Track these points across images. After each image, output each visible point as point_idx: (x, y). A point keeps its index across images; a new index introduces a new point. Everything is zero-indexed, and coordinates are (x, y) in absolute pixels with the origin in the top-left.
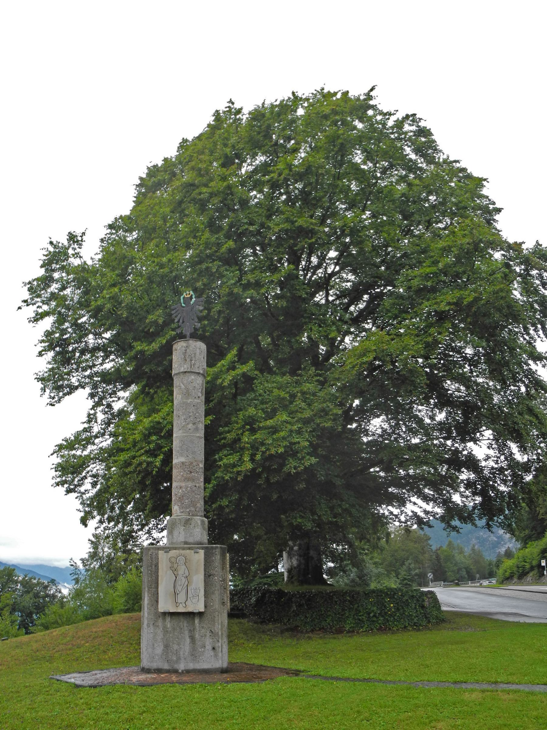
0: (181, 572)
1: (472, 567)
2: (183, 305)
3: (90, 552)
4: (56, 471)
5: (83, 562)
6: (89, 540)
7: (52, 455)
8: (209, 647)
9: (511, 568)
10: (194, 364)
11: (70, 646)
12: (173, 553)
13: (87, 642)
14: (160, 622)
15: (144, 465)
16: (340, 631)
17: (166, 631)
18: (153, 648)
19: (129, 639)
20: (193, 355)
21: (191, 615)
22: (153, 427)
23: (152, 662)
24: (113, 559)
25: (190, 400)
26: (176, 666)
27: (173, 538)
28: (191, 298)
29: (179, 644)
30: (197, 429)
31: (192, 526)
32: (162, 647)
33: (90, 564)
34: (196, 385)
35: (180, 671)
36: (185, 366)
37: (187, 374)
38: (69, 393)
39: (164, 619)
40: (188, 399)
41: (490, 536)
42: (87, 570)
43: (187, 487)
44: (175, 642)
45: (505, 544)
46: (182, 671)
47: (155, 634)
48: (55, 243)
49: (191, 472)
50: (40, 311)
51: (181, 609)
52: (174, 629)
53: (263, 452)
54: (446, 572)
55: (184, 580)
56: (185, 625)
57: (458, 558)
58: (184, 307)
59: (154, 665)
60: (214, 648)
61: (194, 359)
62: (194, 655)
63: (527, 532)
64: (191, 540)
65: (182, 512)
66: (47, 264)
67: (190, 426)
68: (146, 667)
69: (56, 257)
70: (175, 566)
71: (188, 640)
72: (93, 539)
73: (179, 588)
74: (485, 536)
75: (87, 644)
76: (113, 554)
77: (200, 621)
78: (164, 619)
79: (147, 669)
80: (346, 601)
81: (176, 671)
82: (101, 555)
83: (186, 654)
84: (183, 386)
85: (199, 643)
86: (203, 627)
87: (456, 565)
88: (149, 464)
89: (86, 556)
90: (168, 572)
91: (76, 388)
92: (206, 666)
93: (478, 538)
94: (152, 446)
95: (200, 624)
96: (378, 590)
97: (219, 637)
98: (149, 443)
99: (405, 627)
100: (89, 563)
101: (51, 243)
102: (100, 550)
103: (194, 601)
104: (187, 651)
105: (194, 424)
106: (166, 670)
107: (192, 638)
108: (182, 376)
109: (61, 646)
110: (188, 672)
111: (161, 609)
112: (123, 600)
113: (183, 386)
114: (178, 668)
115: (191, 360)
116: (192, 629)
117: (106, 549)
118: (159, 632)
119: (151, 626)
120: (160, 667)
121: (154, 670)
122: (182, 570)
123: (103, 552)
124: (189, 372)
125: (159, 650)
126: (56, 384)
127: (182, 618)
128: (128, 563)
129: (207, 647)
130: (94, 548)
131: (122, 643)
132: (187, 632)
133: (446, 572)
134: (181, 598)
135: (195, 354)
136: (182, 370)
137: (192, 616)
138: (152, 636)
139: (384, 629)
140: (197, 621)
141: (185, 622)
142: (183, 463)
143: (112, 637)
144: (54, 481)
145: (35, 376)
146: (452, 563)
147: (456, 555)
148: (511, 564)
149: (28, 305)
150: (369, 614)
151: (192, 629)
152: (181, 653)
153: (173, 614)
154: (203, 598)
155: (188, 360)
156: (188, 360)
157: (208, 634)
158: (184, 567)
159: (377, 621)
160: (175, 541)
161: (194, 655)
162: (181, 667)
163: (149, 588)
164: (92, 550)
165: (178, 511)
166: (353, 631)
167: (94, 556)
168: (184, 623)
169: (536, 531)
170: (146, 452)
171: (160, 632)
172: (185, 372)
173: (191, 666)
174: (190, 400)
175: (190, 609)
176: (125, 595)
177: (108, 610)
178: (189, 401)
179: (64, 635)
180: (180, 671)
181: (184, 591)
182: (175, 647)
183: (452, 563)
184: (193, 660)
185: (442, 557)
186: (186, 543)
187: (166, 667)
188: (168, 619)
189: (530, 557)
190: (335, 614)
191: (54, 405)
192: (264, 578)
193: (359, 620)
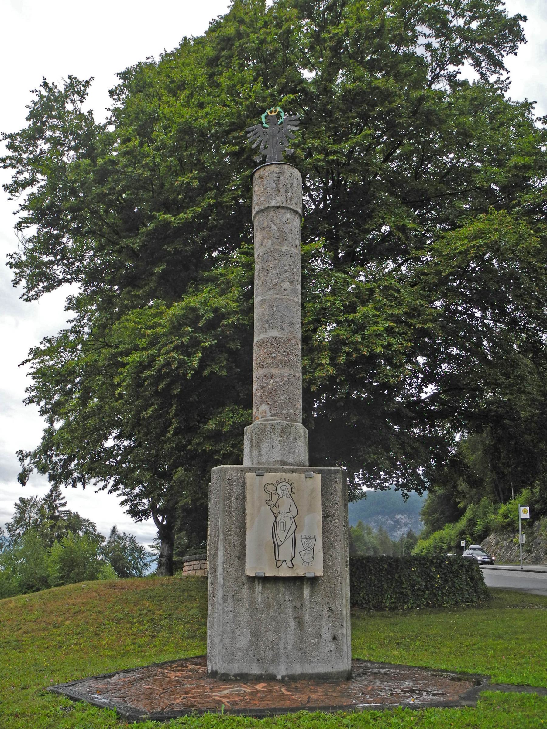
0: (284, 509)
1: (378, 547)
2: (265, 125)
3: (16, 517)
4: (34, 378)
5: (8, 528)
6: (16, 505)
7: (23, 364)
8: (327, 636)
9: (427, 548)
10: (291, 198)
11: (43, 625)
12: (269, 477)
13: (67, 619)
14: (245, 591)
15: (175, 365)
16: (379, 608)
17: (254, 609)
18: (234, 638)
19: (127, 615)
20: (289, 186)
21: (298, 581)
22: (185, 316)
23: (231, 662)
24: (39, 525)
25: (285, 248)
26: (272, 670)
27: (260, 455)
28: (278, 116)
29: (276, 631)
30: (294, 291)
31: (291, 437)
32: (248, 637)
33: (16, 530)
34: (293, 229)
35: (279, 677)
36: (278, 199)
37: (280, 210)
38: (48, 289)
39: (252, 588)
40: (281, 244)
41: (387, 520)
42: (12, 536)
43: (282, 377)
44: (270, 627)
45: (401, 528)
46: (283, 677)
47: (236, 614)
48: (50, 85)
49: (288, 354)
50: (21, 178)
51: (284, 572)
52: (269, 605)
53: (348, 354)
54: (357, 551)
55: (289, 522)
56: (287, 598)
57: (367, 538)
58: (266, 128)
59: (235, 668)
60: (335, 638)
61: (290, 190)
62: (303, 651)
63: (436, 516)
64: (290, 459)
65: (275, 415)
66: (33, 115)
67: (286, 285)
68: (221, 671)
69: (50, 106)
70: (275, 498)
71: (292, 624)
72: (21, 505)
73: (280, 536)
74: (383, 520)
75: (68, 622)
76: (39, 520)
77: (312, 592)
78: (252, 588)
79: (224, 674)
80: (382, 570)
81: (271, 678)
82: (27, 520)
83: (290, 647)
84: (274, 228)
85: (310, 630)
86: (316, 603)
87: (365, 543)
88: (182, 364)
89: (12, 521)
90: (263, 508)
91: (60, 282)
92: (322, 669)
93: (377, 521)
94: (186, 340)
95: (311, 597)
96: (420, 557)
97: (343, 619)
98: (181, 336)
99: (457, 603)
100: (14, 528)
101: (46, 84)
102: (26, 516)
103: (306, 558)
104: (291, 643)
105: (291, 283)
106: (255, 675)
107: (299, 620)
108: (272, 213)
109: (29, 624)
110: (293, 678)
111: (250, 572)
112: (58, 566)
113: (274, 228)
114: (275, 672)
115: (287, 192)
116: (299, 605)
117: (32, 515)
118: (243, 610)
119: (230, 600)
120: (245, 671)
121: (235, 676)
122: (285, 505)
123: (30, 517)
124: (283, 208)
125: (243, 641)
126: (34, 274)
127: (281, 587)
128: (54, 530)
129: (324, 636)
130: (20, 513)
131: (118, 621)
132: (290, 611)
133: (357, 551)
134: (285, 552)
135: (292, 184)
136: (273, 203)
137: (298, 583)
138: (230, 616)
139: (435, 605)
140: (306, 591)
141: (287, 593)
142: (275, 339)
143: (100, 612)
144: (27, 395)
145: (8, 260)
146: (361, 543)
147: (365, 535)
148: (427, 545)
149: (5, 167)
150: (413, 586)
151: (299, 605)
152: (281, 646)
153: (265, 580)
154: (321, 554)
155: (283, 191)
156: (283, 191)
157: (326, 613)
158: (290, 500)
159: (423, 596)
160: (264, 460)
161: (303, 651)
162: (281, 671)
163: (227, 535)
164: (18, 515)
165: (268, 413)
166: (396, 608)
167: (19, 521)
168: (285, 595)
169: (444, 514)
170: (176, 348)
171: (244, 610)
172: (278, 207)
173: (298, 669)
174: (285, 248)
175: (300, 572)
176: (60, 562)
177: (43, 577)
178: (284, 249)
179: (27, 608)
180: (279, 677)
181: (290, 541)
182: (271, 636)
183: (361, 543)
184: (301, 658)
185: (353, 536)
186: (283, 463)
187: (255, 670)
188: (259, 588)
189: (447, 538)
190: (370, 586)
191: (30, 301)
192: (199, 548)
193: (402, 593)
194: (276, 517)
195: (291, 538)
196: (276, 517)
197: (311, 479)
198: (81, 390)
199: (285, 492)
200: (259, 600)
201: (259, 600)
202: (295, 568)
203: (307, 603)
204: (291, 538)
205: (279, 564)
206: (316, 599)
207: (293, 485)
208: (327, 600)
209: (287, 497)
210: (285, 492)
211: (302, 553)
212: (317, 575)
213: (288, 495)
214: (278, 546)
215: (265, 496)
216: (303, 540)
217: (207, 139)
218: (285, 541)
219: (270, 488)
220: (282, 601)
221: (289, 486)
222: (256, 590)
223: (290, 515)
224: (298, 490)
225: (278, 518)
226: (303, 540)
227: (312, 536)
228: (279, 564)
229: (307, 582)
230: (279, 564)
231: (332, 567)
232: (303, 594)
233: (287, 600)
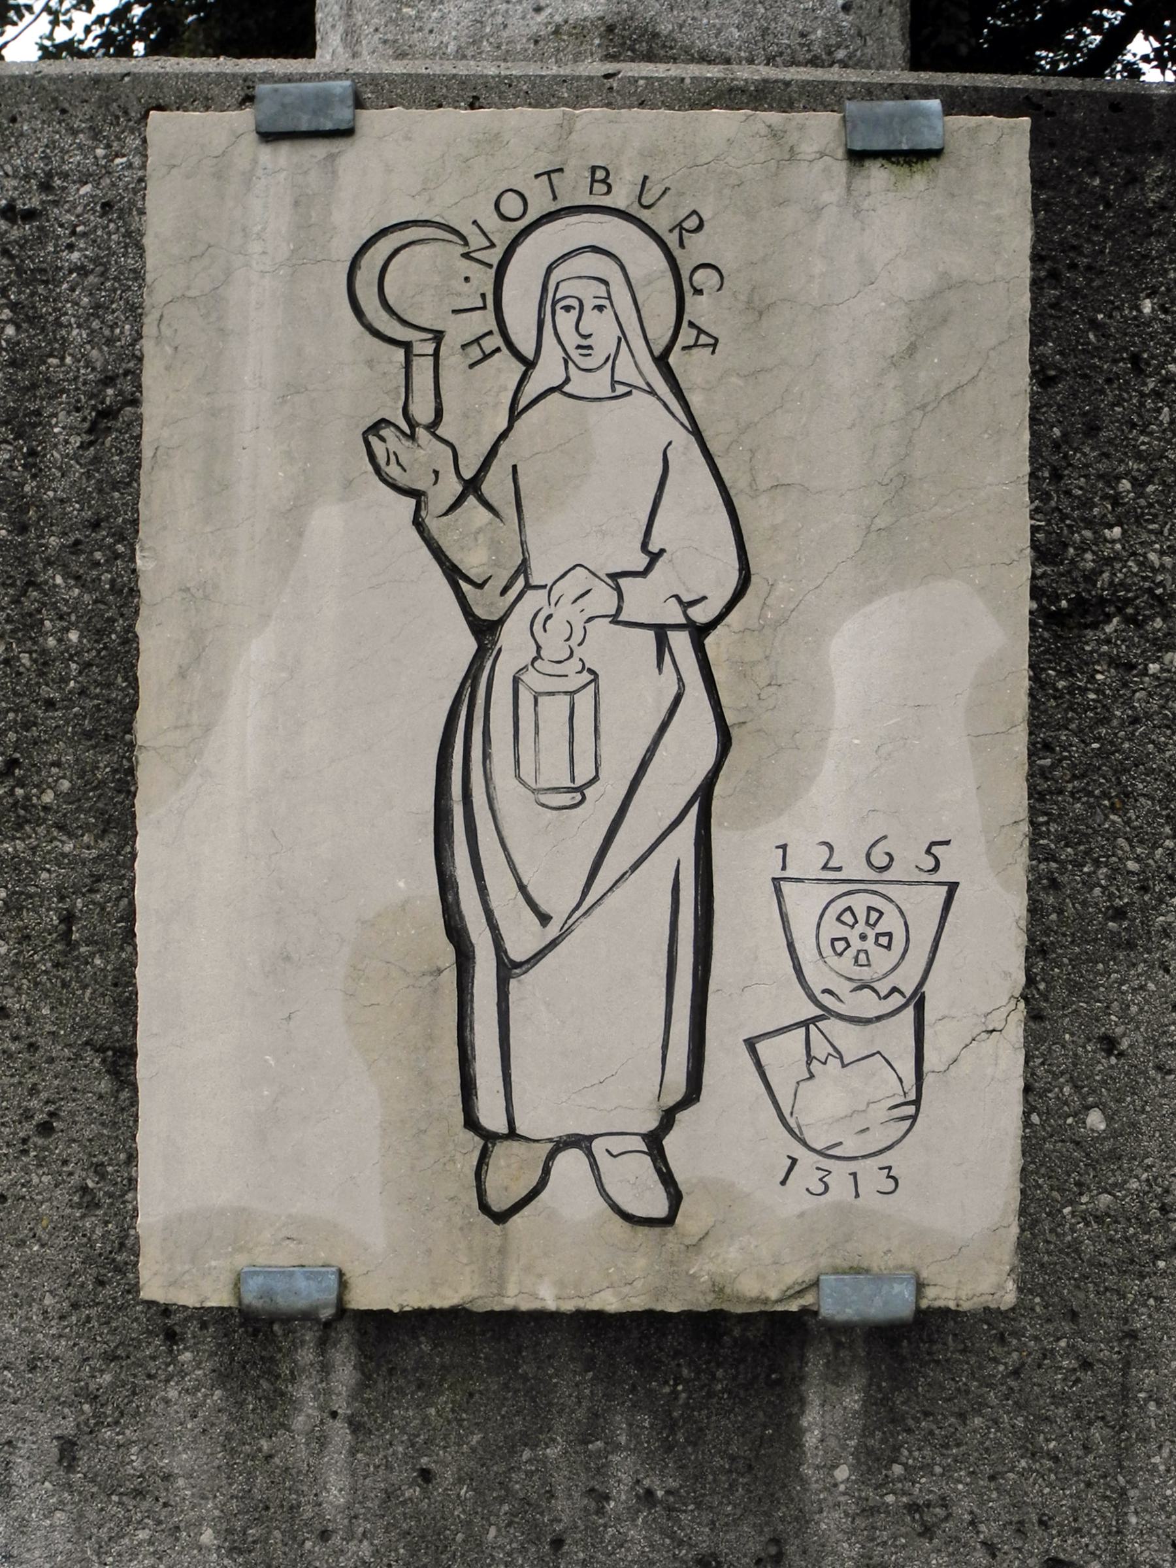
55: (637, 685)
70: (476, 399)
73: (536, 845)
90: (328, 520)
95: (872, 1463)
103: (825, 1105)
134: (584, 1039)
154: (1003, 1063)
158: (650, 422)
181: (643, 909)
194: (485, 631)
195: (659, 870)
196: (485, 631)
197: (919, 179)
198: (1119, 62)
199: (602, 329)
200: (335, 1494)
201: (335, 1494)
202: (691, 1219)
203: (829, 1522)
204: (659, 870)
205: (509, 1175)
206: (924, 1488)
207: (698, 248)
208: (1036, 1491)
209: (620, 391)
210: (602, 329)
211: (782, 1054)
212: (940, 1296)
213: (636, 366)
214: (507, 969)
215: (361, 379)
216: (805, 904)
217: (1072, 562)
218: (583, 908)
219: (425, 282)
220: (566, 1509)
221: (646, 260)
222: (303, 1391)
223: (649, 600)
224: (758, 309)
225: (514, 641)
226: (805, 904)
227: (910, 858)
228: (505, 1183)
229: (835, 1376)
230: (505, 1183)
231: (1108, 1156)
232: (794, 1441)
233: (621, 1495)
